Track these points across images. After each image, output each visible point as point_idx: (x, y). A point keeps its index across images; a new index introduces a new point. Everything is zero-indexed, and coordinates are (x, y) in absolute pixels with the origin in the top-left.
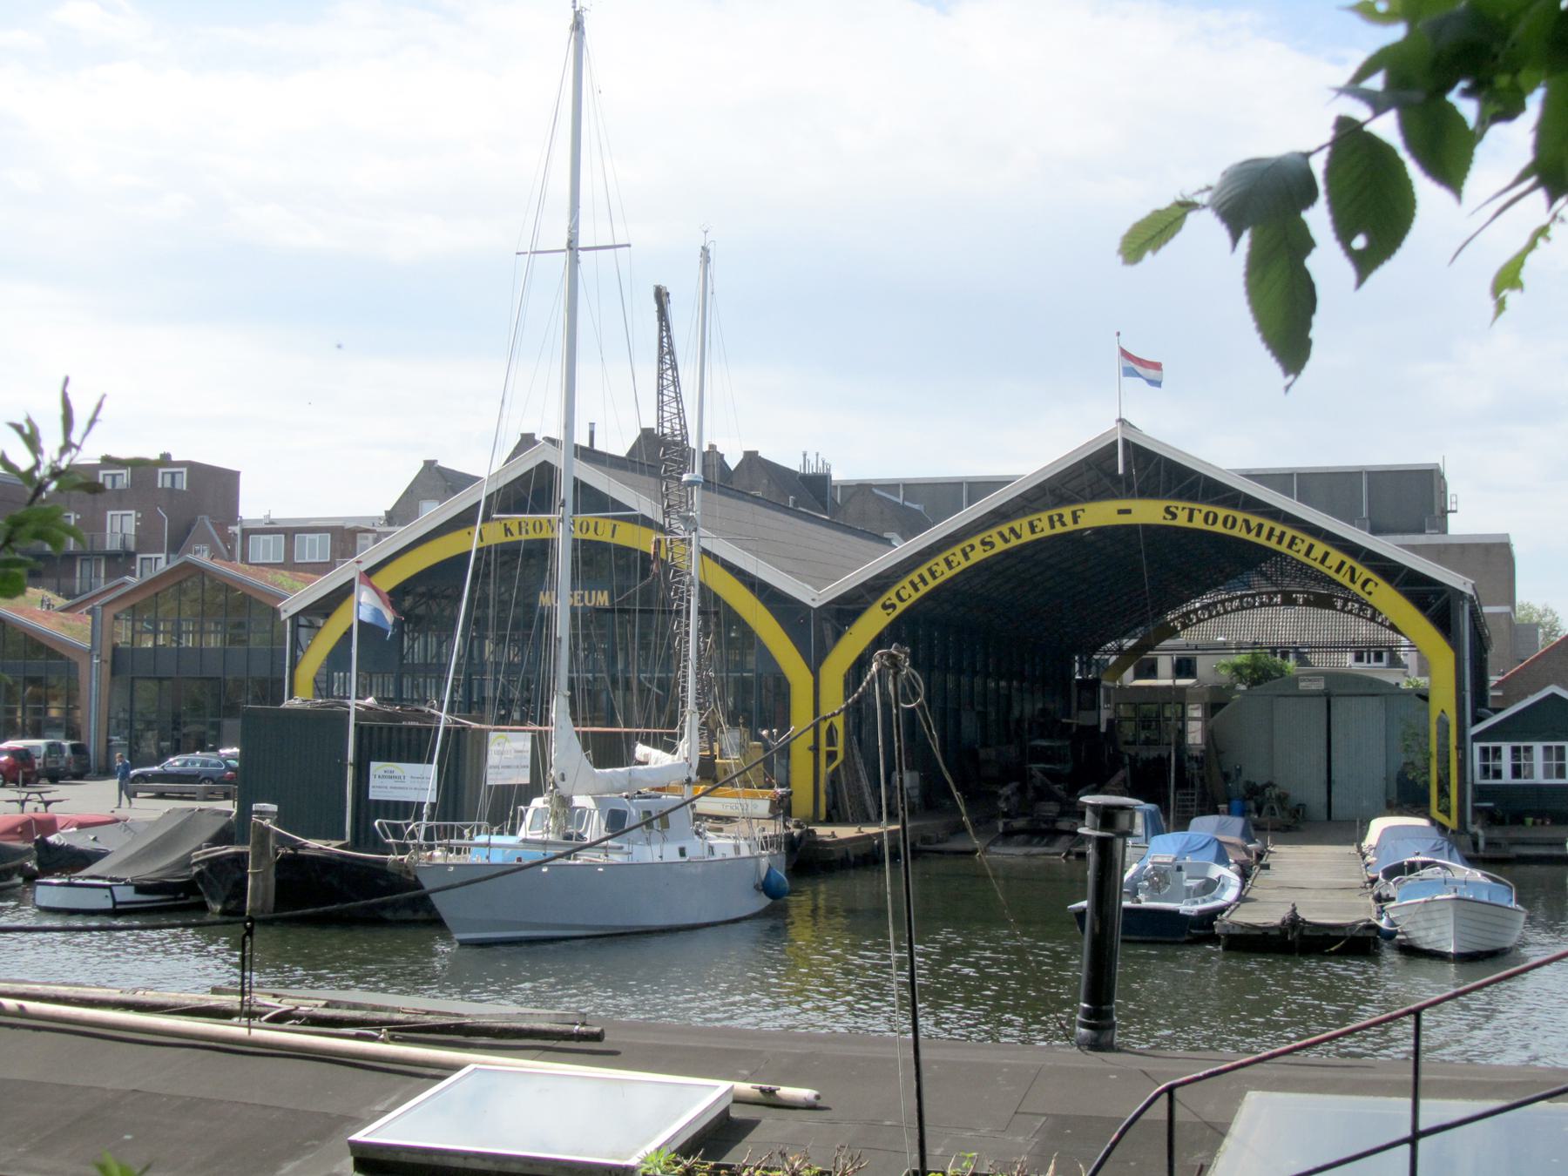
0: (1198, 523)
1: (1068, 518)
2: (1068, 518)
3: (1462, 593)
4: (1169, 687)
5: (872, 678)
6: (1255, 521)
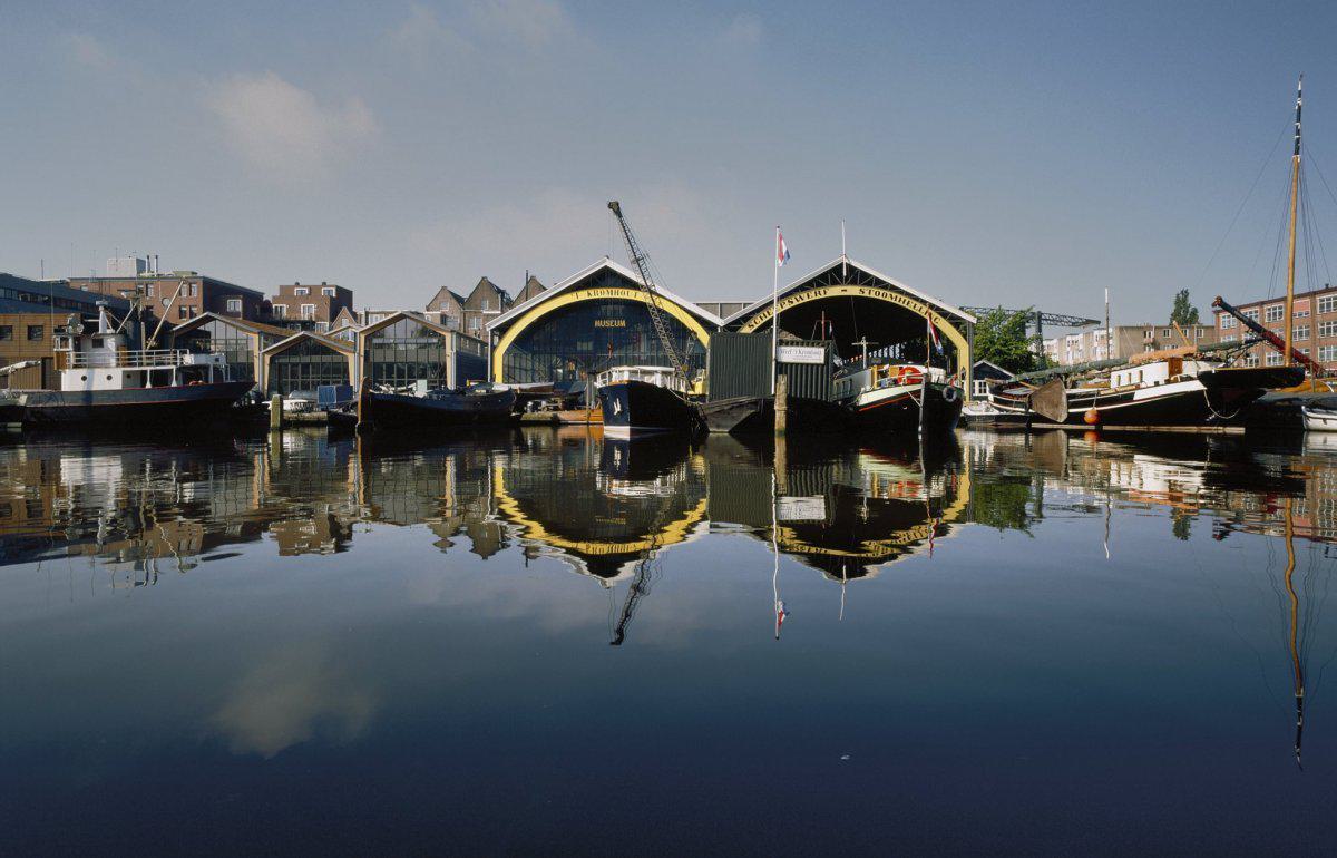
0: (873, 295)
1: (822, 292)
2: (822, 292)
3: (645, 304)
4: (829, 548)
5: (1009, 377)
6: (894, 295)
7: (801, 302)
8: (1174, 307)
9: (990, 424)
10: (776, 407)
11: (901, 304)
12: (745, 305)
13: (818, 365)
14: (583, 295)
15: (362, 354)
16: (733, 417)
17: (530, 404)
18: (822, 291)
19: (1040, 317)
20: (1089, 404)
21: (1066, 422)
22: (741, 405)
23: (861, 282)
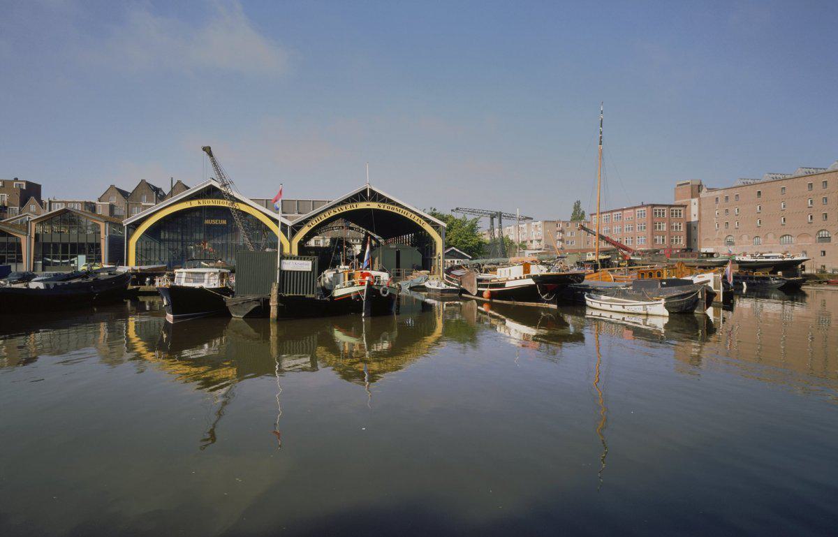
0: (386, 209)
1: (355, 206)
2: (355, 206)
6: (399, 209)
7: (342, 211)
8: (573, 210)
9: (438, 294)
10: (271, 304)
11: (403, 214)
12: (329, 202)
13: (307, 272)
14: (195, 203)
15: (33, 236)
16: (245, 309)
17: (148, 279)
18: (355, 205)
19: (500, 215)
20: (486, 286)
21: (476, 296)
22: (249, 301)
23: (379, 199)
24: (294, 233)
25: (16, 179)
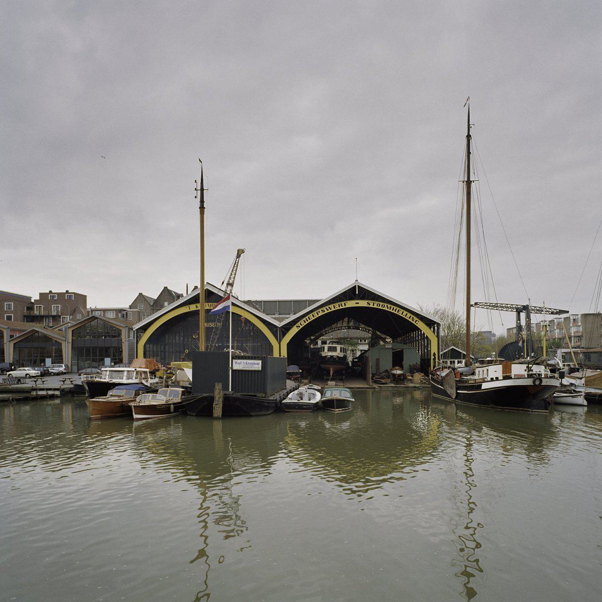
0: (375, 306)
1: (343, 305)
2: (343, 305)
6: (389, 306)
18: (343, 303)
24: (284, 334)
25: (51, 292)
